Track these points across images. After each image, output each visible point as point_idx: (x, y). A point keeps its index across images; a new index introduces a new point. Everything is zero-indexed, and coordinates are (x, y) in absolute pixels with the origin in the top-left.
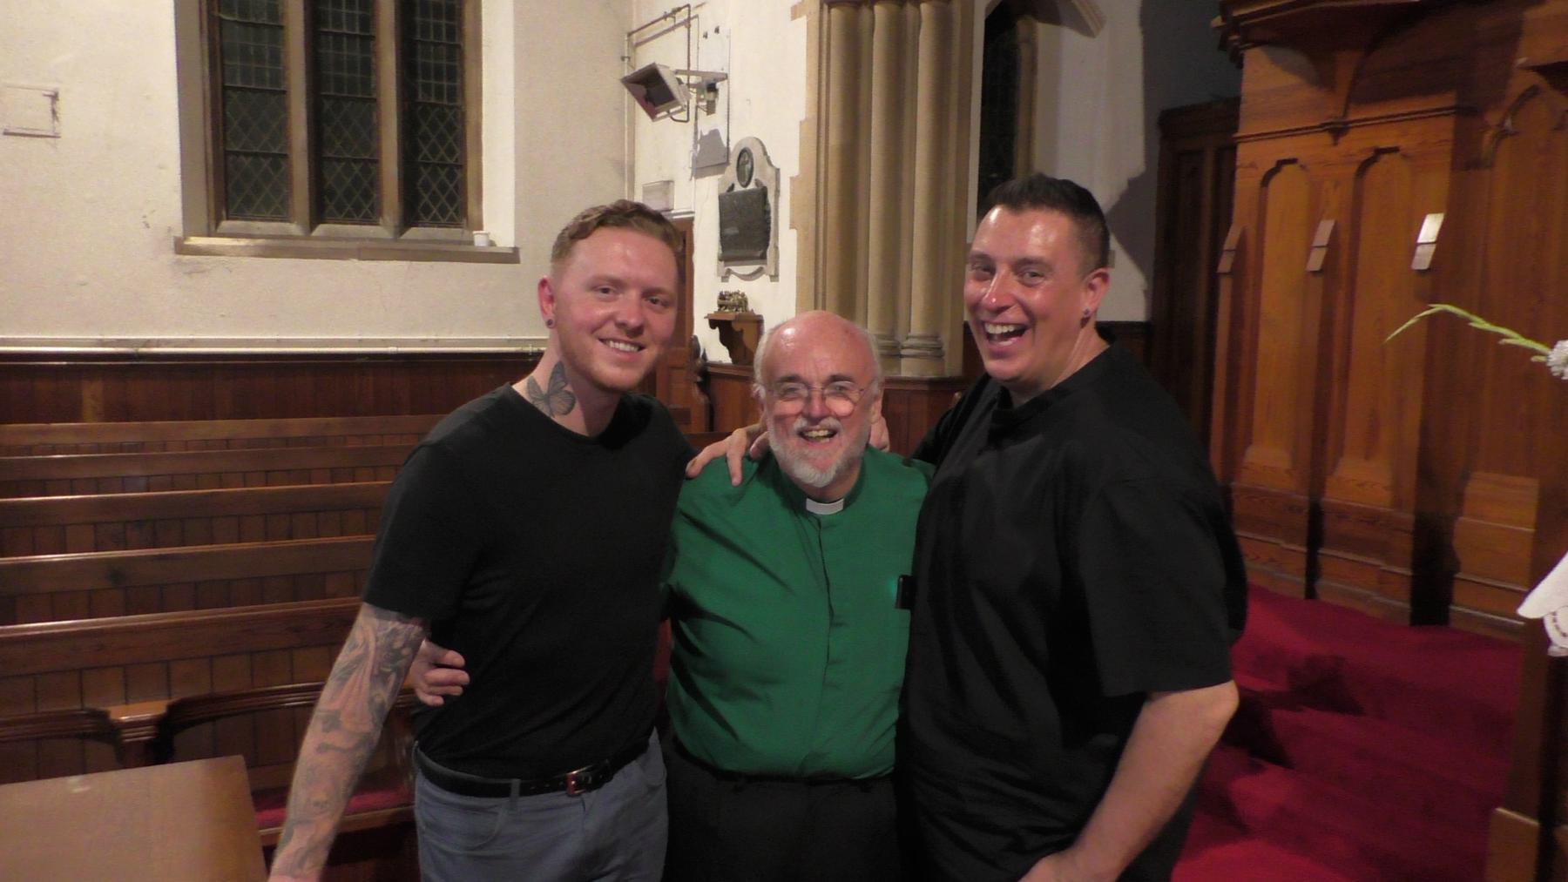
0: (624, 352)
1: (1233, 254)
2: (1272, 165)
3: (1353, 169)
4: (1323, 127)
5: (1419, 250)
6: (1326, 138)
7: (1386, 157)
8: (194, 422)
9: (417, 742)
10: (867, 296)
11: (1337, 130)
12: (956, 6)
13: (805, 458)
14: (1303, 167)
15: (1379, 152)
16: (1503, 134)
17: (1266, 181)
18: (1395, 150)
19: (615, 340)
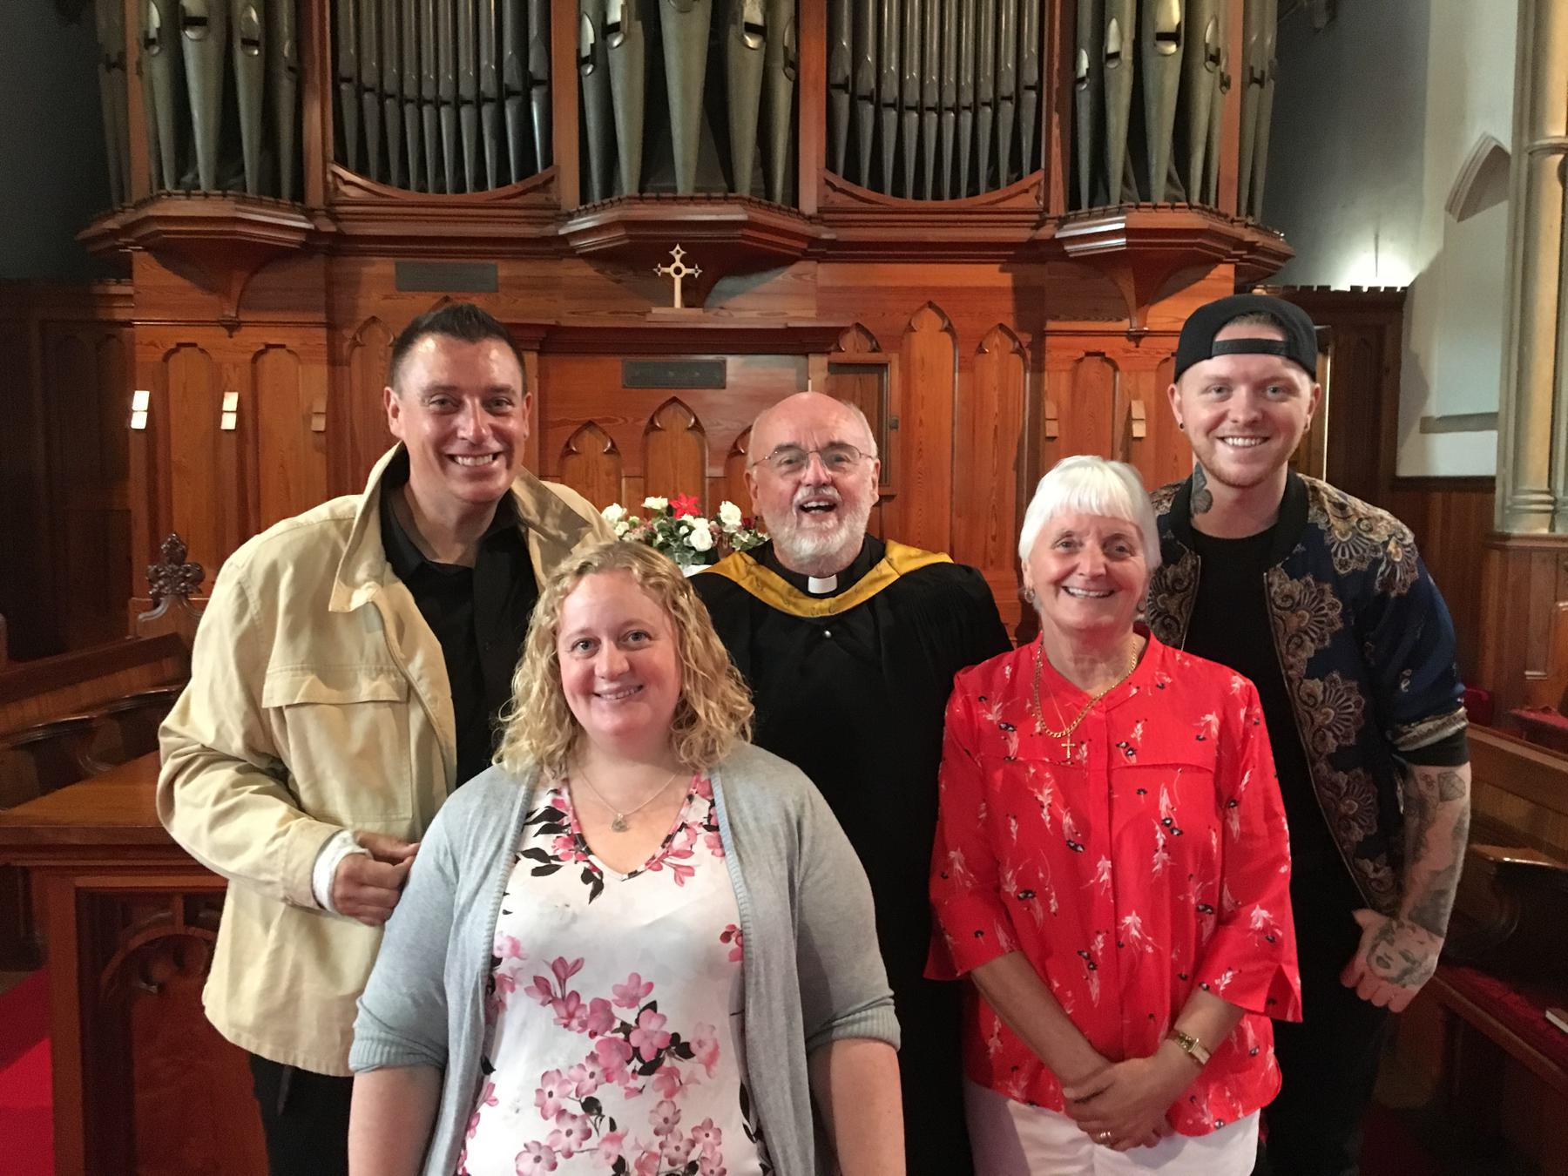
0: (1244, 447)
1: (225, 408)
2: (173, 346)
3: (249, 357)
4: (220, 323)
5: (323, 409)
6: (224, 332)
7: (272, 351)
8: (733, 1048)
9: (1038, 729)
10: (1518, 383)
11: (233, 327)
12: (947, 2)
13: (791, 527)
14: (202, 351)
15: (269, 346)
16: (355, 344)
17: (166, 358)
18: (282, 346)
19: (1233, 437)
